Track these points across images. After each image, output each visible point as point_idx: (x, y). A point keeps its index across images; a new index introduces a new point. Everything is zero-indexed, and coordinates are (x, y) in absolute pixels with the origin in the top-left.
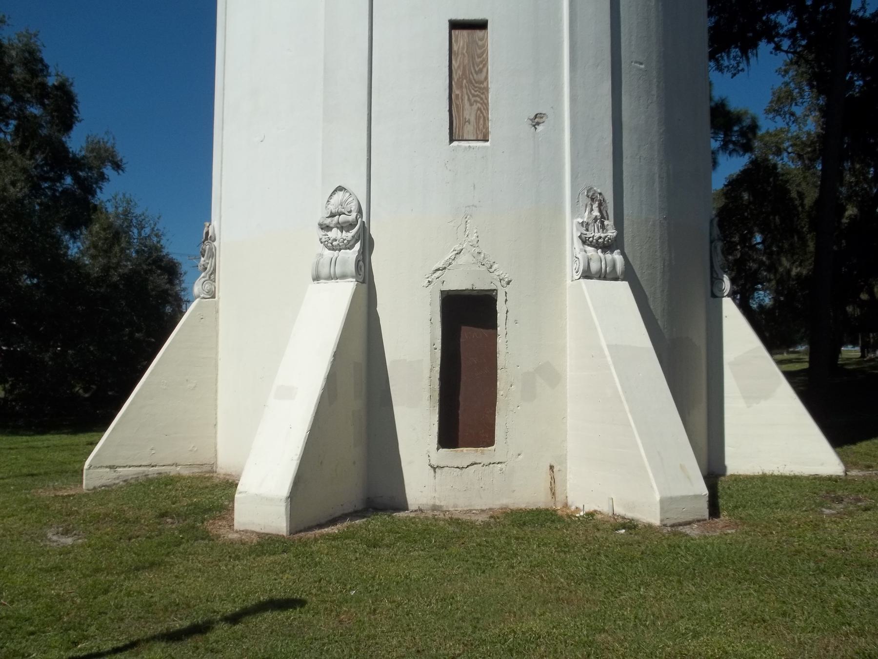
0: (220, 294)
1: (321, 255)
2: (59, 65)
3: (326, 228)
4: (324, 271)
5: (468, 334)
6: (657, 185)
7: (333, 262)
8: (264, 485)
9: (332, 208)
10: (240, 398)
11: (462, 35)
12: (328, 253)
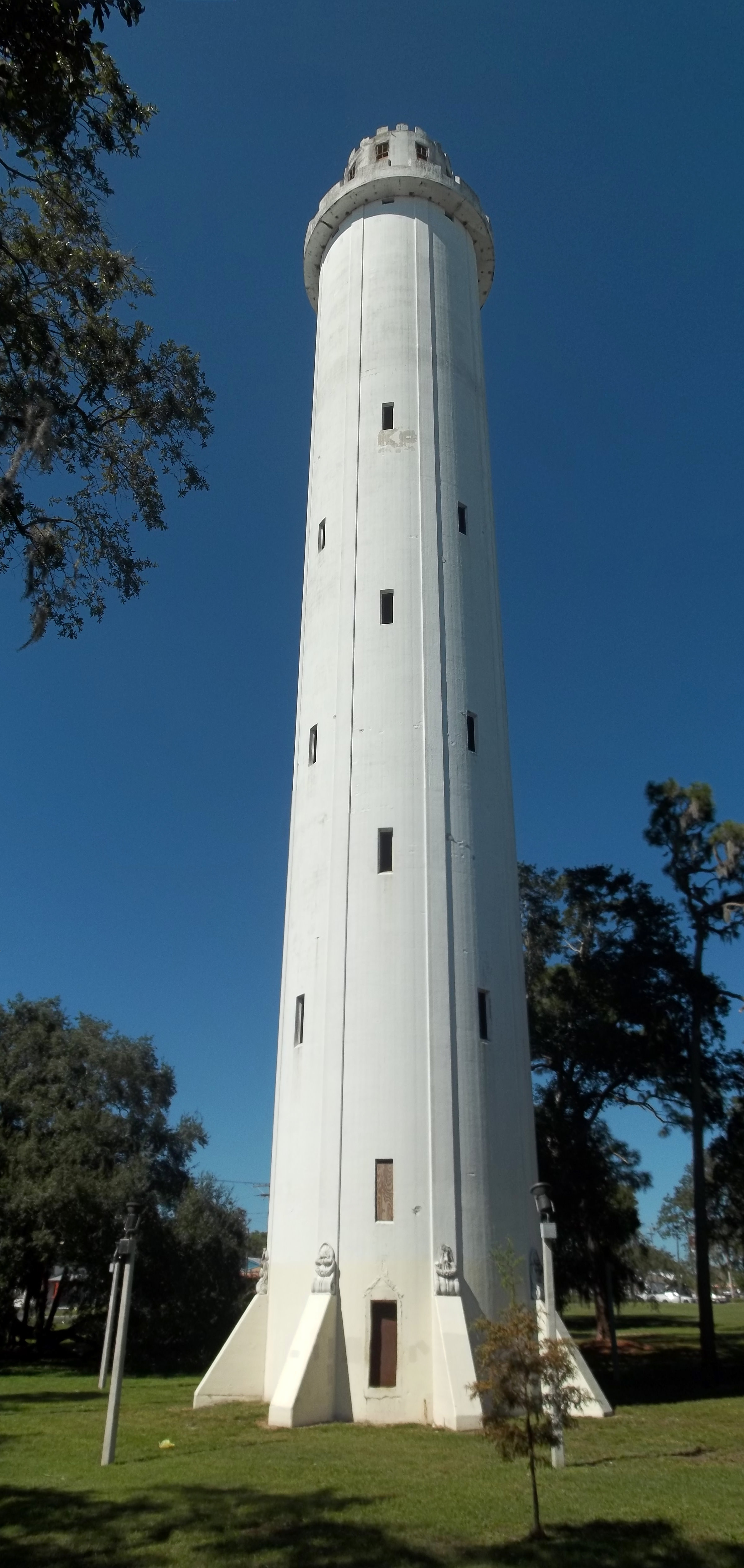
0: (270, 1291)
1: (316, 1279)
2: (166, 1056)
3: (318, 1264)
4: (317, 1288)
5: (385, 1323)
6: (484, 1239)
7: (321, 1283)
8: (281, 1402)
9: (322, 1254)
10: (268, 1359)
11: (382, 1166)
12: (319, 1278)
